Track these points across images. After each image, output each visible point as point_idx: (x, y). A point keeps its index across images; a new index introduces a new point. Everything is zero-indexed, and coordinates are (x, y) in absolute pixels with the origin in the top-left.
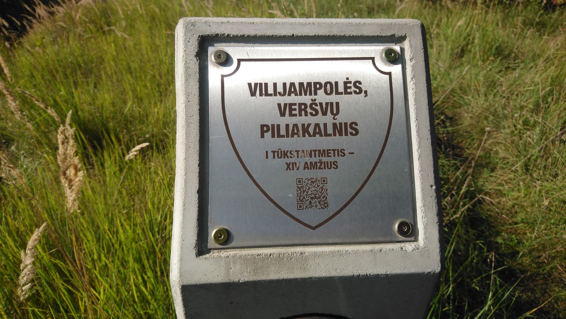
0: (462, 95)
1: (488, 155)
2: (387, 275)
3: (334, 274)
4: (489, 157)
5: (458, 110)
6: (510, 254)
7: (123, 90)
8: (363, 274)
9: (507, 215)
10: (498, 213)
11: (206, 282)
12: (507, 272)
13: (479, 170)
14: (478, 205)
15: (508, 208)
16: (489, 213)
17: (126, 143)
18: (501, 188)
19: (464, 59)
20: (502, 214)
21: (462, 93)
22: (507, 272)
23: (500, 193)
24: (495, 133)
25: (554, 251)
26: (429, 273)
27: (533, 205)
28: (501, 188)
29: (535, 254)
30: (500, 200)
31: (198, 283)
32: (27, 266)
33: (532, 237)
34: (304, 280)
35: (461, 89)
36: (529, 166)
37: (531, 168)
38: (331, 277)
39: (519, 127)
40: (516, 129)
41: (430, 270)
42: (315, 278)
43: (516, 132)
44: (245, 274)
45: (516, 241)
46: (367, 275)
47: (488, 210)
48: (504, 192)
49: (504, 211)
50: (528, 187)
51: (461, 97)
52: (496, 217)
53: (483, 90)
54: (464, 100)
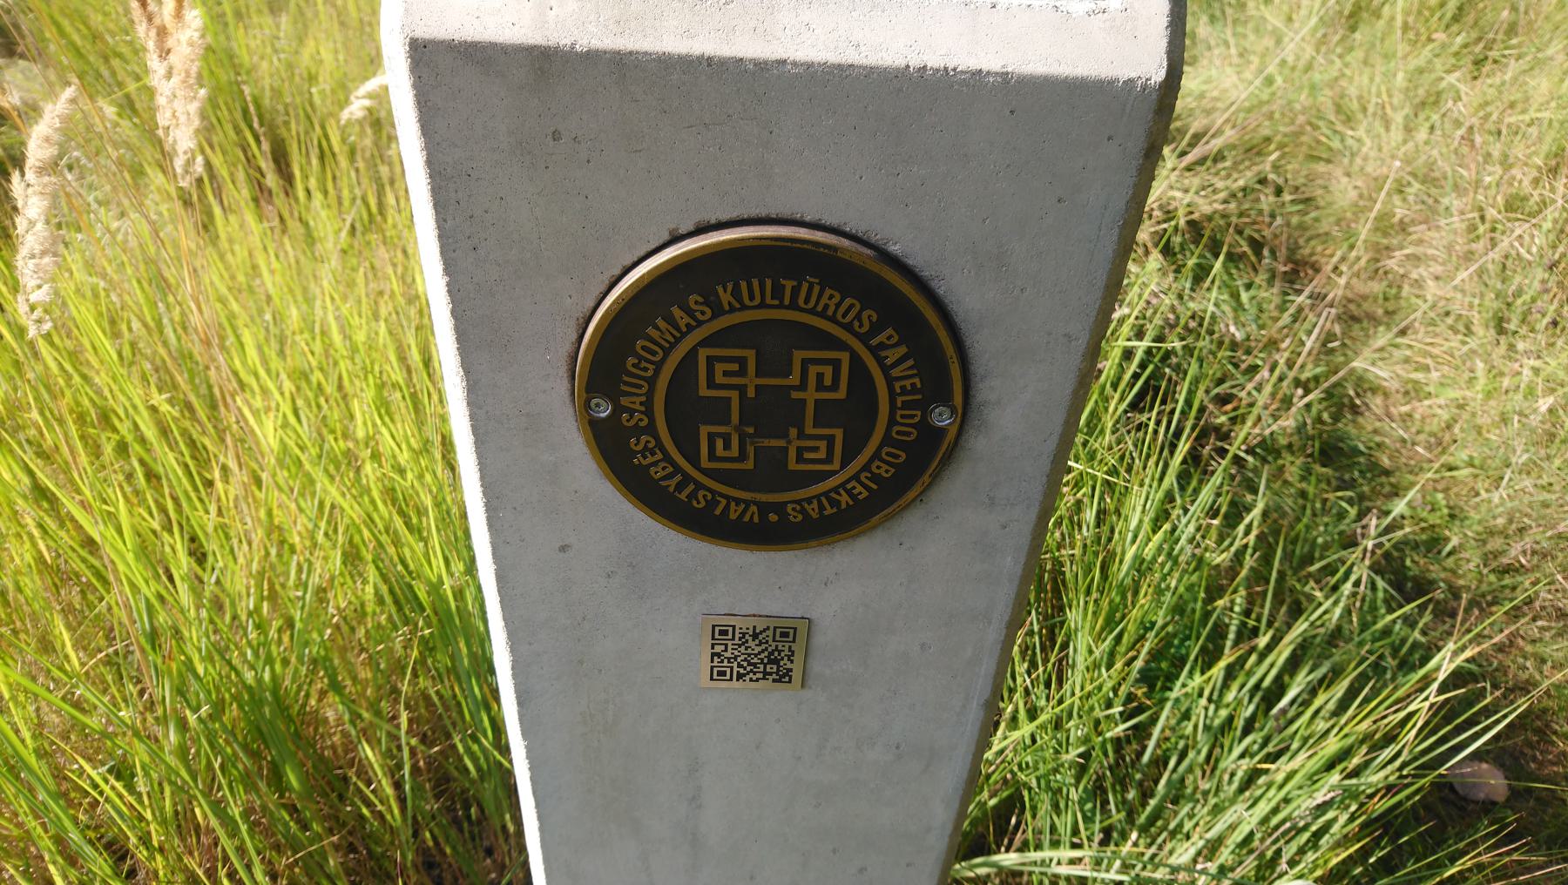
0: (1339, 127)
1: (1394, 291)
2: (1005, 75)
3: (851, 56)
4: (1398, 297)
5: (1321, 168)
6: (1425, 542)
7: (373, 53)
8: (936, 66)
9: (1429, 448)
10: (1404, 441)
11: (477, 38)
12: (1409, 585)
13: (1362, 329)
14: (1349, 416)
15: (1435, 428)
16: (1378, 439)
17: (368, 154)
18: (1419, 376)
19: (1357, 35)
20: (1414, 444)
21: (1344, 123)
22: (1409, 585)
23: (1413, 391)
24: (1423, 227)
25: (1549, 533)
26: (1130, 82)
27: (1505, 420)
28: (1419, 376)
29: (1496, 544)
30: (1413, 409)
31: (457, 37)
32: (32, 223)
33: (1495, 503)
34: (762, 66)
35: (1339, 109)
36: (1509, 321)
37: (1512, 327)
38: (840, 67)
39: (1491, 213)
40: (1482, 218)
41: (1133, 75)
42: (795, 64)
43: (1481, 229)
44: (592, 28)
45: (1446, 511)
46: (946, 69)
47: (1375, 431)
48: (1427, 389)
49: (1422, 437)
50: (1495, 373)
51: (1335, 132)
52: (1397, 451)
53: (1398, 118)
54: (1342, 141)
